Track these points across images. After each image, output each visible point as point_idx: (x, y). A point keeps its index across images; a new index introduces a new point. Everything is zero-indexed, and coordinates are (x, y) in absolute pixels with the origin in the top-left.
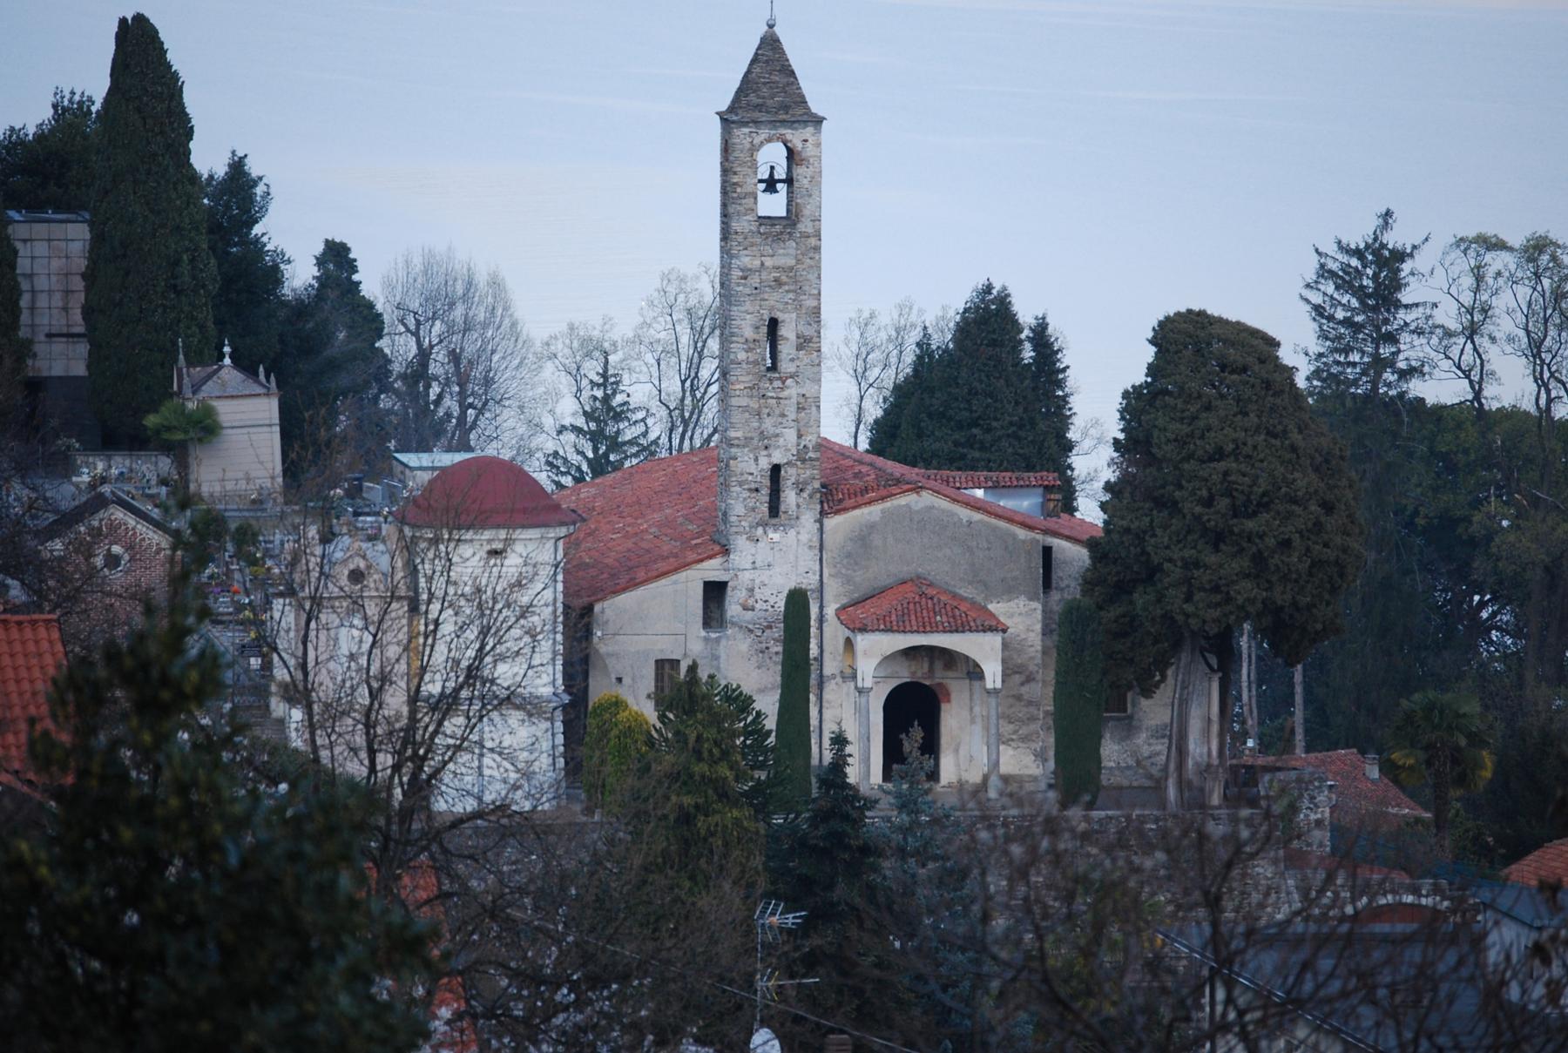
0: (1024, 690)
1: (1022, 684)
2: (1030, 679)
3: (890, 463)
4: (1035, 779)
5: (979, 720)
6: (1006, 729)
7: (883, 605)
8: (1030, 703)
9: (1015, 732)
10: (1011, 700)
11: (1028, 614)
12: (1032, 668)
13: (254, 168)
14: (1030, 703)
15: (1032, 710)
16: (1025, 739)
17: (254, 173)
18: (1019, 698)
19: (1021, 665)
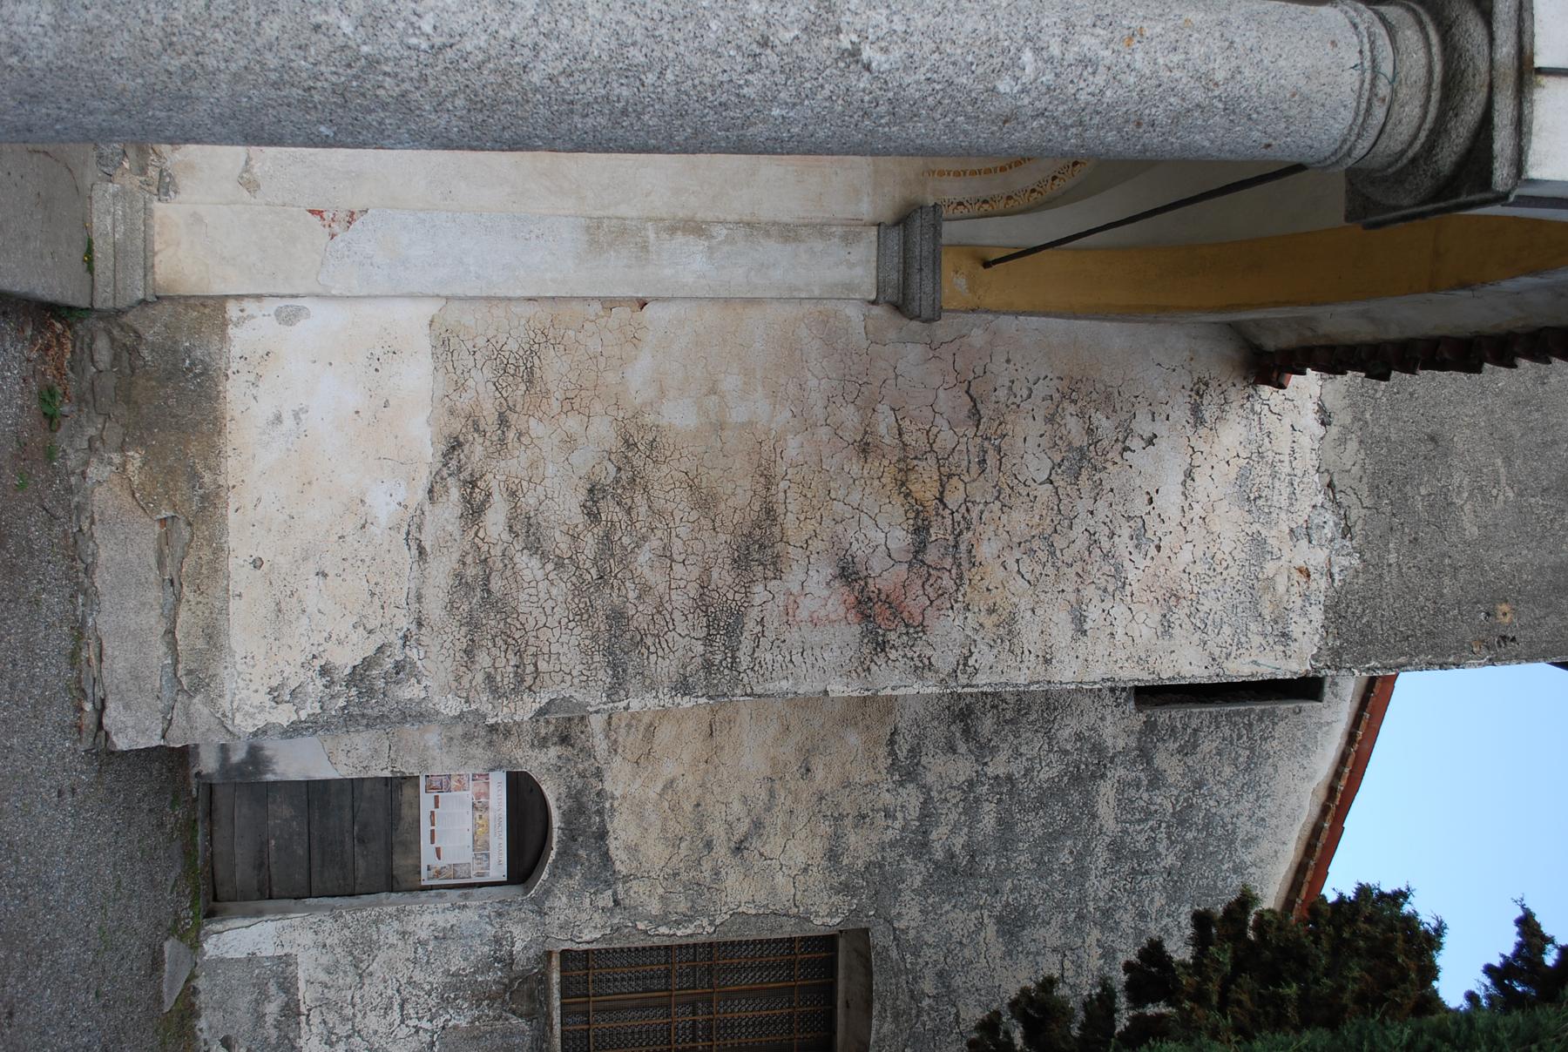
0: (811, 587)
1: (848, 573)
2: (877, 615)
3: (1497, 146)
4: (193, 676)
5: (615, 274)
6: (551, 471)
7: (1022, 179)
8: (723, 624)
9: (528, 531)
10: (739, 496)
11: (1255, 588)
12: (947, 632)
13: (1446, 940)
14: (723, 624)
15: (684, 642)
16: (481, 600)
17: (1427, 919)
18: (757, 549)
19: (963, 560)
